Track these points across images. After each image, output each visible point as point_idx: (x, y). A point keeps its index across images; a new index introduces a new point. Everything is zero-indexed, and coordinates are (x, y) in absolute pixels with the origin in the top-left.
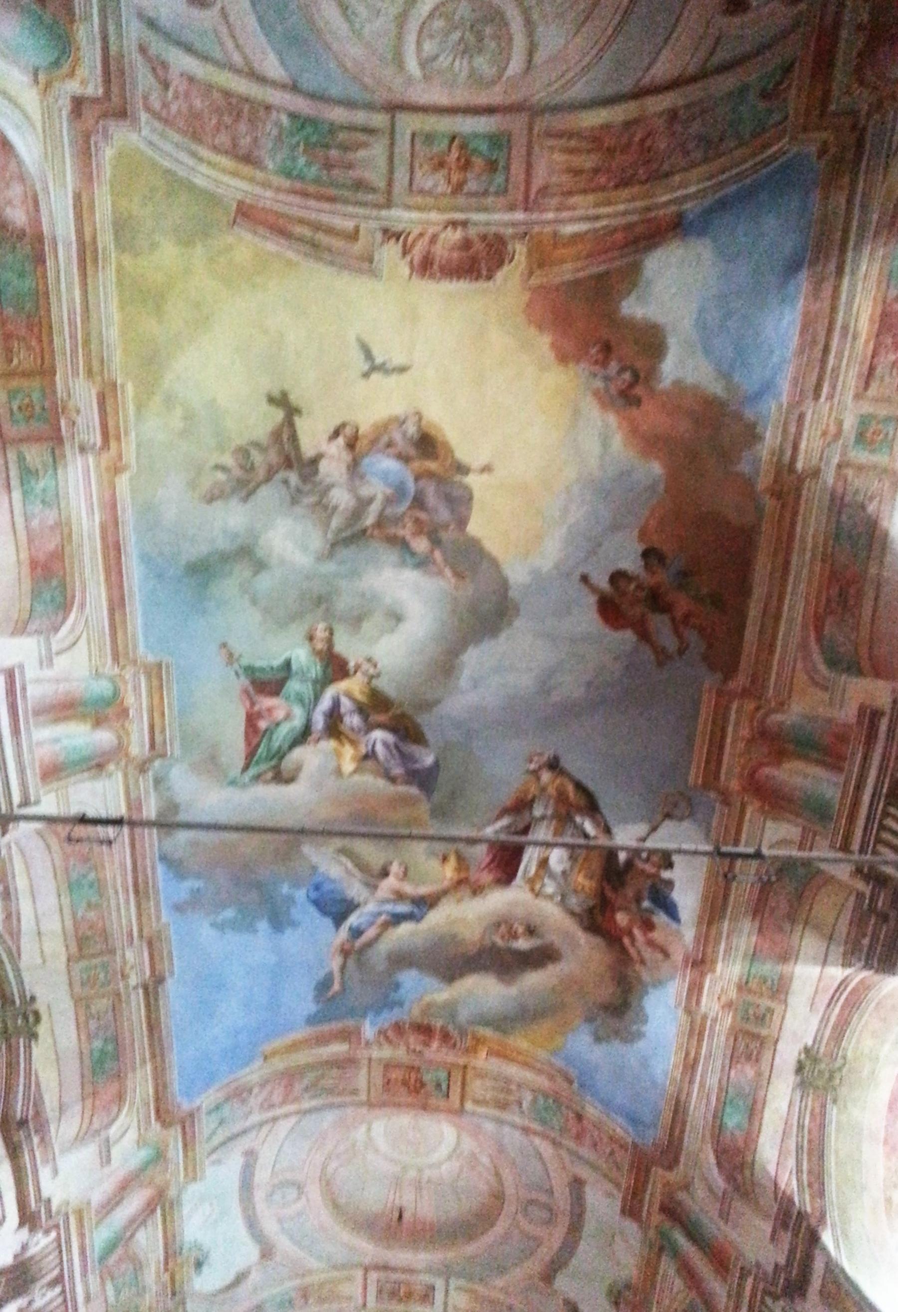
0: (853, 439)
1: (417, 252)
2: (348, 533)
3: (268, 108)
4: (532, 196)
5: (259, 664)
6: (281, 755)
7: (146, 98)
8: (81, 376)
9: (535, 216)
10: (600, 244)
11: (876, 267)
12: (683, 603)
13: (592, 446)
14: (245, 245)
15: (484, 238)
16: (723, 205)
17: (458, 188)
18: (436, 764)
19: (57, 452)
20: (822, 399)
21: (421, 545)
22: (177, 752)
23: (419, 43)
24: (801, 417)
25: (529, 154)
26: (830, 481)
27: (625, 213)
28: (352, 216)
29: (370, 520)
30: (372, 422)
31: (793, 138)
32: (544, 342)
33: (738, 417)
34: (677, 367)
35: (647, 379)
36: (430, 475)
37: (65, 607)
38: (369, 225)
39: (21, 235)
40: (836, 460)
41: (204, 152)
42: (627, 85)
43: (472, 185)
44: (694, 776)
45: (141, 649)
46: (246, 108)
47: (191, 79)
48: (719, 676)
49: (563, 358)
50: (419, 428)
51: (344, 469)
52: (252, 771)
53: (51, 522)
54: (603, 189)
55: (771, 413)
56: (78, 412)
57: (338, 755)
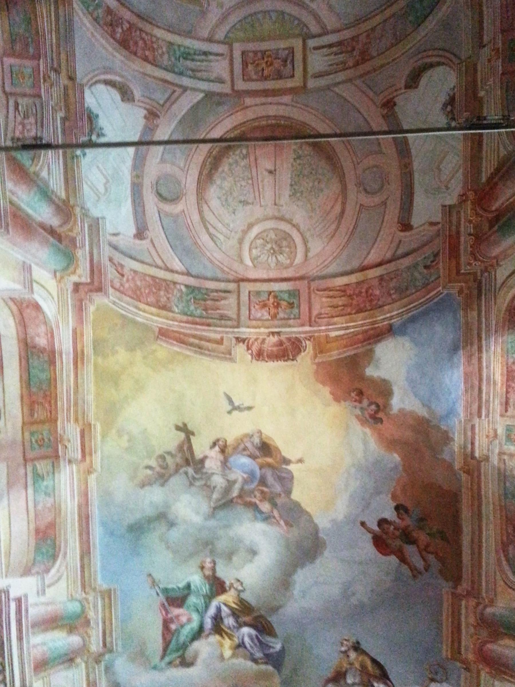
0: (504, 438)
1: (255, 348)
2: (223, 501)
3: (175, 283)
4: (313, 319)
5: (170, 586)
6: (184, 647)
7: (112, 281)
8: (72, 421)
9: (315, 328)
10: (351, 340)
11: (499, 350)
12: (423, 537)
13: (359, 447)
14: (163, 350)
15: (289, 339)
16: (413, 320)
17: (274, 317)
18: (283, 650)
19: (55, 464)
20: (483, 417)
21: (265, 507)
22: (120, 649)
23: (250, 250)
24: (473, 427)
25: (310, 298)
26: (496, 462)
27: (362, 325)
28: (220, 332)
29: (235, 493)
30: (234, 438)
31: (444, 287)
32: (326, 391)
33: (438, 428)
34: (401, 401)
35: (385, 407)
36: (269, 465)
37: (54, 557)
38: (228, 335)
39: (42, 351)
40: (497, 451)
41: (142, 306)
42: (355, 264)
43: (281, 315)
44: (446, 652)
45: (99, 581)
46: (164, 284)
47: (135, 272)
48: (451, 584)
49: (337, 399)
50: (261, 439)
51: (219, 464)
52: (167, 659)
53: (49, 505)
54: (350, 314)
55: (456, 426)
56: (69, 441)
57: (221, 645)
